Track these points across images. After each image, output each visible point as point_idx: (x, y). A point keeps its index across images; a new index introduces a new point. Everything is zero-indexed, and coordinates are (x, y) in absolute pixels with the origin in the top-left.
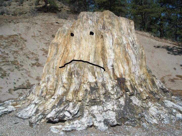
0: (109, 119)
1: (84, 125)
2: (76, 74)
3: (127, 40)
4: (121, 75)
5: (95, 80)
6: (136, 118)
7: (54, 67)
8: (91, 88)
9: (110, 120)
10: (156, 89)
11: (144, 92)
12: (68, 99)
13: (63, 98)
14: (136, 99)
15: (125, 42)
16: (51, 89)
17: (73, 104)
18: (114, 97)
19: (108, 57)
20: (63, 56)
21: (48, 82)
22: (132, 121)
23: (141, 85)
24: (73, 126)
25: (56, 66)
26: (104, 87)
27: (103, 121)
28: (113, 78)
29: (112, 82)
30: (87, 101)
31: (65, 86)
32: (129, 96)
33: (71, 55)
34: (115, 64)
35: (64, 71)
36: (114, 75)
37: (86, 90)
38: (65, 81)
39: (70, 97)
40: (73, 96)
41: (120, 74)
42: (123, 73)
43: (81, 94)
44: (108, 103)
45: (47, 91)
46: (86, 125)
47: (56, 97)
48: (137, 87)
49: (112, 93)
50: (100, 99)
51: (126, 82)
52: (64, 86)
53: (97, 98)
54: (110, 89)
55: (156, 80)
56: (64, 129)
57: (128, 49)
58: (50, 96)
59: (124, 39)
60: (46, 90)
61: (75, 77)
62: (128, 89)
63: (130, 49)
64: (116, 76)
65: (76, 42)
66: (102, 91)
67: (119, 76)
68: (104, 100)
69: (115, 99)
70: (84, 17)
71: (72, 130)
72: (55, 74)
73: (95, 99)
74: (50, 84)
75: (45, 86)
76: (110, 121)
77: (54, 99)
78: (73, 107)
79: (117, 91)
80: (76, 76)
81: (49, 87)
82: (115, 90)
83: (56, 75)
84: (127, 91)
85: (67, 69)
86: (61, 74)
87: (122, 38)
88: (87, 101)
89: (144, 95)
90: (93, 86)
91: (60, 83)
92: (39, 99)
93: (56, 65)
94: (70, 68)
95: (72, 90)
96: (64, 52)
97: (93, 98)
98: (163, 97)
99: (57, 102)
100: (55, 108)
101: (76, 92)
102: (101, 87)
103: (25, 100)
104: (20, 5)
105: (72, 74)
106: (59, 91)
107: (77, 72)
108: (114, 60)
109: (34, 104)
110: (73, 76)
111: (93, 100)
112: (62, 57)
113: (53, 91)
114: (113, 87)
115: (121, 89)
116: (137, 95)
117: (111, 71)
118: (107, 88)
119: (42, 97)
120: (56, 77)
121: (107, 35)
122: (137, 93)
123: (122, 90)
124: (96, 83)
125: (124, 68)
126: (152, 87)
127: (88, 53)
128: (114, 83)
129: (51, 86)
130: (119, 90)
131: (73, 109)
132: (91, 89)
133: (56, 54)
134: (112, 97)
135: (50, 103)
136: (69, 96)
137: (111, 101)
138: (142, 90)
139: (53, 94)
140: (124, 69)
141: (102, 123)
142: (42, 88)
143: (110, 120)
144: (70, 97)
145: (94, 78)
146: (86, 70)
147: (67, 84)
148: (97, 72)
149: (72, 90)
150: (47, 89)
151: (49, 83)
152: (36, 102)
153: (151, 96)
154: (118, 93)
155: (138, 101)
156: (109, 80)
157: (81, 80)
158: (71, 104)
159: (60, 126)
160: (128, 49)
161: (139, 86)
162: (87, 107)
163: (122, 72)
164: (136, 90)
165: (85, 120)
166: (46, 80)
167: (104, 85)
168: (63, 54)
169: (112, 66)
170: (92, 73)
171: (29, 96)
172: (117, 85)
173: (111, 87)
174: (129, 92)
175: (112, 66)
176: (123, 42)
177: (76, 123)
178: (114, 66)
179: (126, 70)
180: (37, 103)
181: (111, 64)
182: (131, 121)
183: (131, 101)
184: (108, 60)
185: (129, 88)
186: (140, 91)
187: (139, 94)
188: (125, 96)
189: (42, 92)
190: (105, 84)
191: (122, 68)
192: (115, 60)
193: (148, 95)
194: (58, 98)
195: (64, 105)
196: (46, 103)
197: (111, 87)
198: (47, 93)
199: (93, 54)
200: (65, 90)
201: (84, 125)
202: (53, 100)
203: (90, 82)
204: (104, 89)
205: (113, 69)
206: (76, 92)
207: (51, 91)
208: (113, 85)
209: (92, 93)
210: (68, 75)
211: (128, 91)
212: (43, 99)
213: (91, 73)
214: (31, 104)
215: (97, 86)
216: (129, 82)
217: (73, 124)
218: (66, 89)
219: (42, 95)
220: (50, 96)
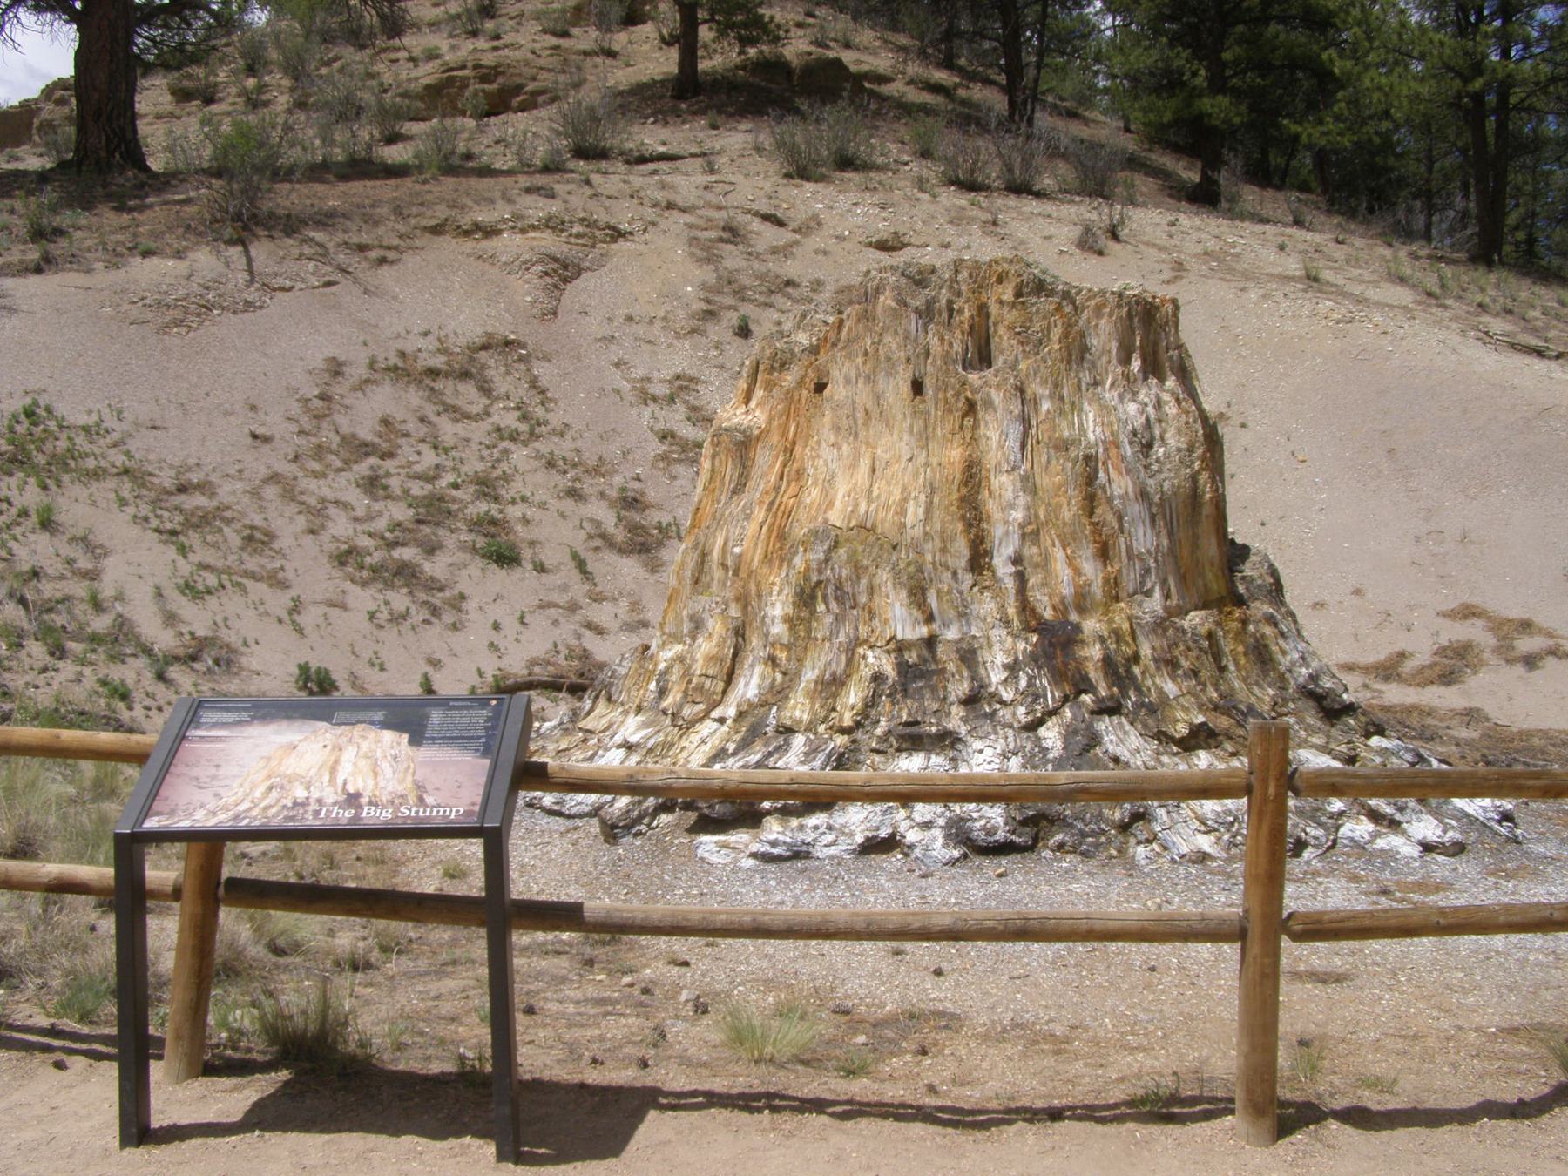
0: (975, 815)
1: (852, 835)
2: (836, 598)
3: (1111, 424)
4: (1061, 608)
5: (924, 631)
6: (1106, 821)
7: (729, 562)
8: (903, 668)
9: (975, 820)
10: (1271, 692)
11: (1181, 700)
12: (788, 723)
13: (767, 716)
14: (1126, 733)
15: (1094, 432)
16: (710, 672)
17: (809, 742)
18: (1014, 714)
19: (997, 515)
20: (772, 503)
21: (694, 639)
22: (1083, 835)
23: (1173, 665)
24: (800, 837)
25: (740, 555)
26: (969, 668)
27: (942, 822)
28: (1016, 623)
29: (1010, 640)
30: (879, 732)
31: (782, 656)
32: (1092, 713)
33: (812, 495)
34: (1031, 551)
35: (777, 580)
36: (1025, 607)
37: (878, 678)
38: (778, 629)
39: (797, 714)
40: (812, 708)
41: (1056, 600)
42: (1069, 600)
43: (853, 696)
44: (978, 745)
45: (690, 682)
46: (860, 839)
47: (731, 712)
48: (1143, 673)
49: (1007, 695)
50: (938, 724)
51: (1083, 642)
52: (772, 661)
53: (927, 719)
54: (996, 677)
55: (1281, 642)
56: (755, 847)
57: (1106, 471)
58: (702, 707)
59: (1091, 415)
60: (684, 676)
61: (828, 610)
62: (1085, 678)
63: (1120, 473)
64: (1033, 610)
65: (837, 429)
66: (960, 688)
67: (1048, 614)
68: (963, 730)
69: (1016, 725)
70: (882, 298)
71: (796, 856)
72: (730, 595)
73: (916, 723)
74: (705, 646)
75: (681, 659)
76: (978, 825)
77: (722, 720)
78: (807, 754)
79: (1030, 684)
80: (834, 605)
81: (701, 662)
82: (1023, 683)
83: (737, 599)
84: (1082, 687)
85: (793, 572)
86: (759, 596)
87: (1081, 410)
88: (879, 732)
89: (1180, 714)
90: (912, 657)
91: (755, 641)
92: (645, 725)
93: (737, 550)
94: (808, 569)
95: (809, 675)
96: (781, 478)
97: (909, 715)
98: (1303, 733)
99: (737, 737)
100: (723, 760)
101: (832, 685)
102: (951, 667)
103: (567, 732)
104: (474, 34)
105: (813, 597)
106: (747, 685)
107: (839, 587)
108: (1029, 529)
109: (619, 747)
110: (821, 607)
111: (907, 724)
112: (769, 510)
113: (721, 685)
114: (1012, 669)
115: (1058, 676)
116: (1136, 713)
117: (1010, 584)
118: (983, 672)
119: (664, 712)
120: (734, 611)
121: (997, 397)
122: (1140, 705)
123: (1056, 683)
124: (931, 642)
125: (1077, 572)
126: (1245, 680)
127: (897, 495)
128: (1021, 645)
129: (711, 659)
130: (1045, 682)
131: (803, 763)
132: (899, 673)
133: (738, 489)
134: (1004, 713)
135: (703, 741)
136: (795, 708)
137: (996, 733)
138: (1170, 688)
139: (718, 697)
140: (1080, 575)
141: (938, 833)
142: (662, 666)
143: (975, 820)
144: (799, 708)
145: (920, 617)
146: (884, 576)
147: (788, 647)
148: (938, 591)
149: (809, 675)
150: (687, 674)
151: (700, 640)
152: (633, 739)
153: (1223, 722)
154: (1036, 698)
155: (1134, 740)
156: (998, 633)
157: (857, 629)
158: (799, 741)
159: (740, 837)
160: (1106, 471)
161: (1158, 668)
162: (877, 758)
163: (1067, 590)
164: (1138, 690)
165: (862, 817)
166: (686, 627)
167: (968, 656)
168: (777, 488)
169: (1017, 560)
170: (911, 594)
171: (588, 713)
172: (1034, 658)
173: (1006, 667)
174: (1094, 694)
175: (1017, 560)
176: (1083, 431)
177: (816, 828)
178: (1026, 563)
179: (1088, 584)
180: (638, 745)
181: (1009, 550)
182: (1081, 831)
183: (1094, 740)
184: (998, 531)
185: (1095, 675)
186: (1161, 692)
187: (1152, 709)
188: (1068, 714)
189: (662, 693)
190: (973, 652)
191: (1068, 571)
192: (1030, 532)
193: (1201, 719)
194: (741, 715)
195: (766, 744)
196: (684, 743)
197: (1006, 667)
198: (685, 692)
199: (922, 497)
200: (779, 677)
201: (852, 835)
202: (715, 725)
203: (899, 637)
204: (966, 674)
205: (1021, 578)
206: (832, 685)
207: (708, 683)
208: (1016, 659)
209: (905, 691)
210: (794, 604)
211: (1089, 688)
212: (668, 721)
213: (904, 594)
214: (607, 749)
215: (936, 661)
216: (1098, 646)
217: (801, 827)
218: (784, 674)
219: (664, 704)
220: (702, 707)
